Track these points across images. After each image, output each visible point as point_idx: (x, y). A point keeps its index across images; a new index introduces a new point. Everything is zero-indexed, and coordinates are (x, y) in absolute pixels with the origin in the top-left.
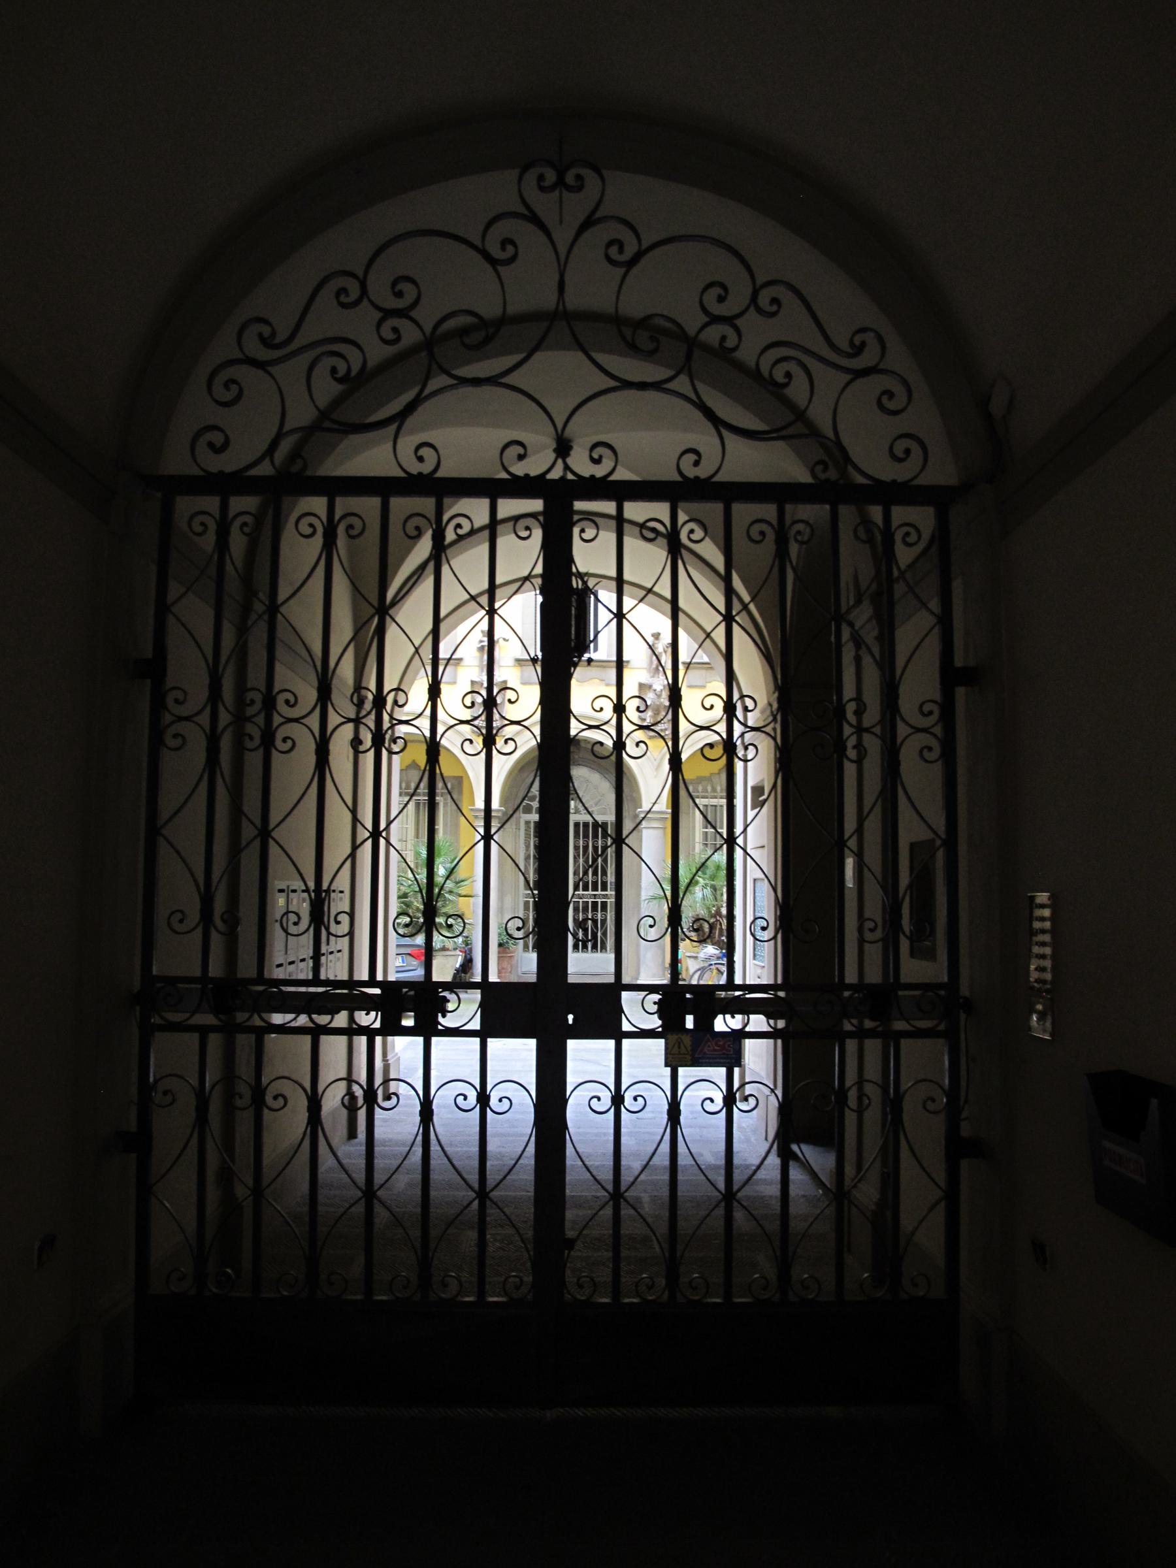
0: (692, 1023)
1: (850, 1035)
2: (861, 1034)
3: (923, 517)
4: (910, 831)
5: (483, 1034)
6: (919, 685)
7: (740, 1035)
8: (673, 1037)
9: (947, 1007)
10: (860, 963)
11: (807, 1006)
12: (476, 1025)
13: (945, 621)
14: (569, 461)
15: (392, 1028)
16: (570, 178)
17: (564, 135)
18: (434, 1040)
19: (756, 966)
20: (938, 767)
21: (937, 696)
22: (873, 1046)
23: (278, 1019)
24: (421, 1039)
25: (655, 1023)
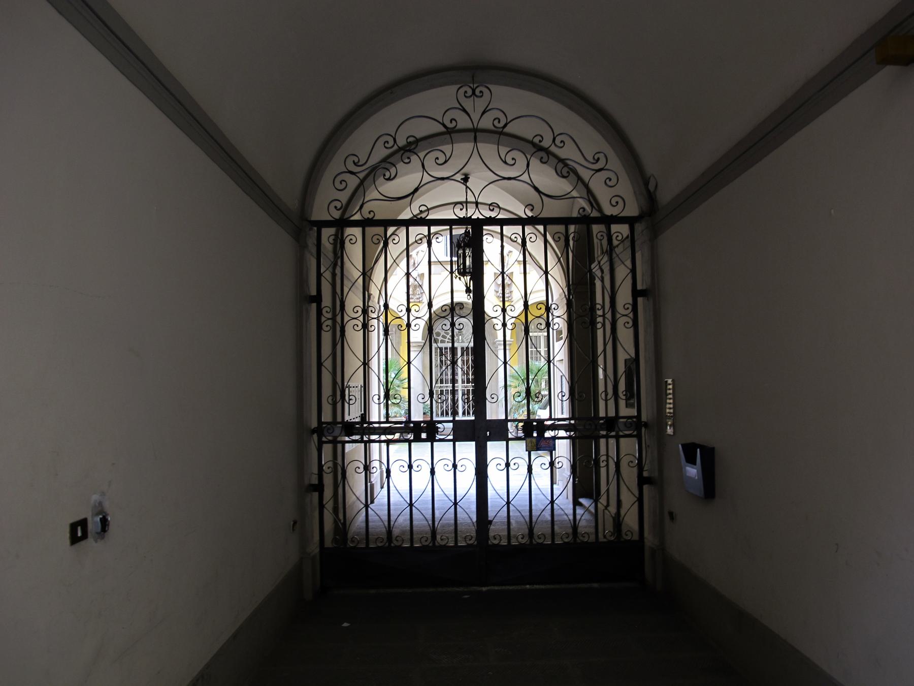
0: (536, 435)
1: (603, 436)
2: (607, 437)
3: (624, 229)
4: (622, 357)
5: (454, 441)
6: (624, 296)
7: (554, 438)
8: (529, 440)
9: (637, 425)
10: (604, 409)
11: (586, 427)
12: (451, 437)
13: (633, 271)
14: (468, 184)
15: (418, 439)
16: (477, 92)
17: (475, 73)
18: (435, 443)
19: (561, 410)
20: (631, 330)
21: (631, 302)
22: (612, 442)
23: (373, 437)
24: (429, 444)
25: (521, 434)
